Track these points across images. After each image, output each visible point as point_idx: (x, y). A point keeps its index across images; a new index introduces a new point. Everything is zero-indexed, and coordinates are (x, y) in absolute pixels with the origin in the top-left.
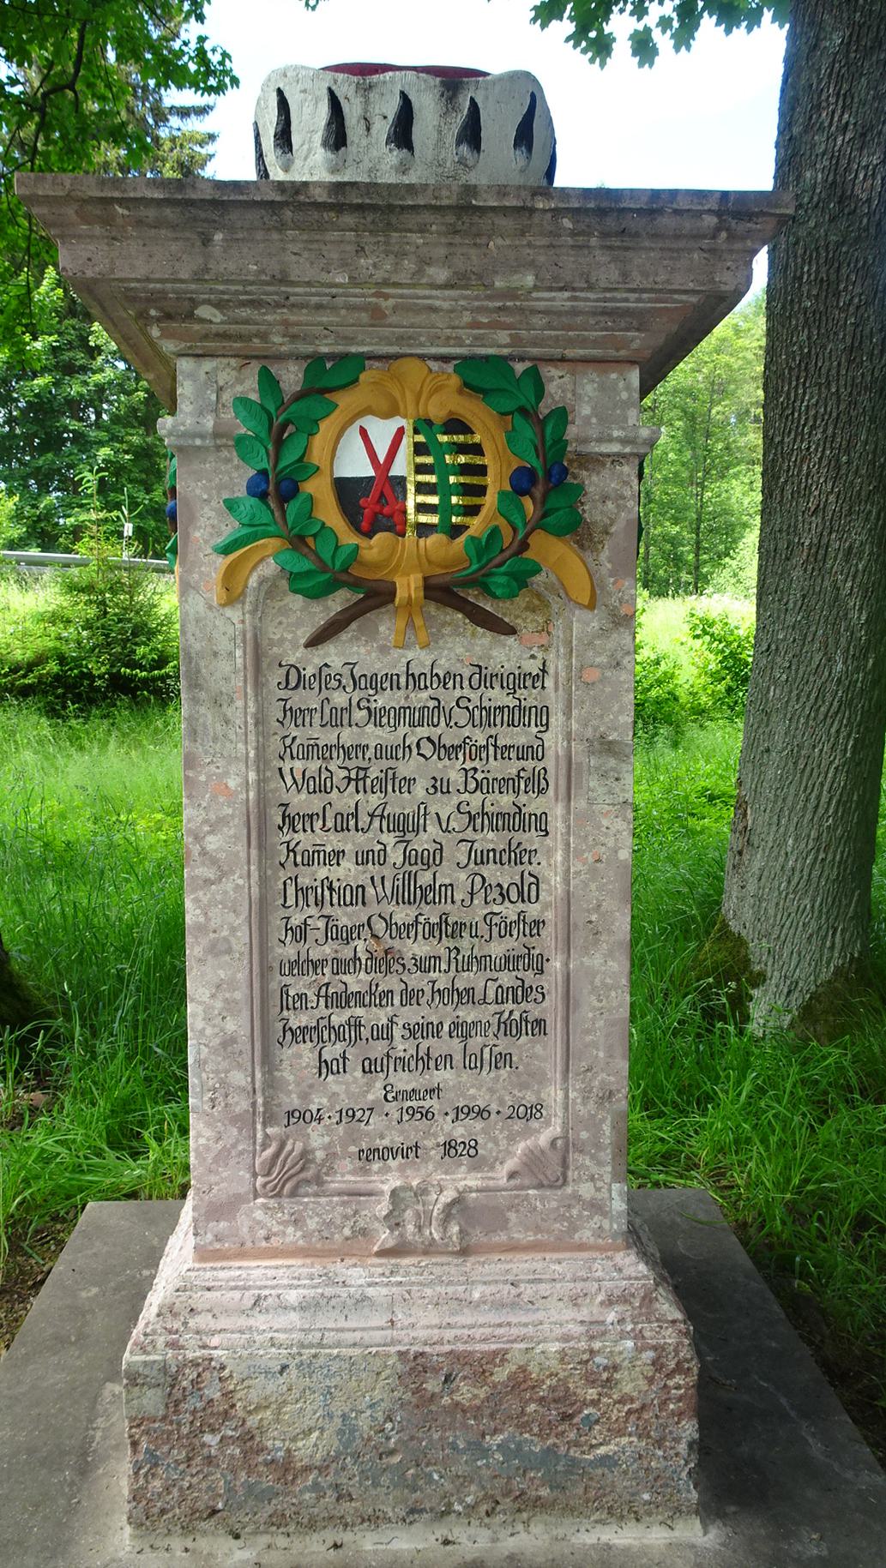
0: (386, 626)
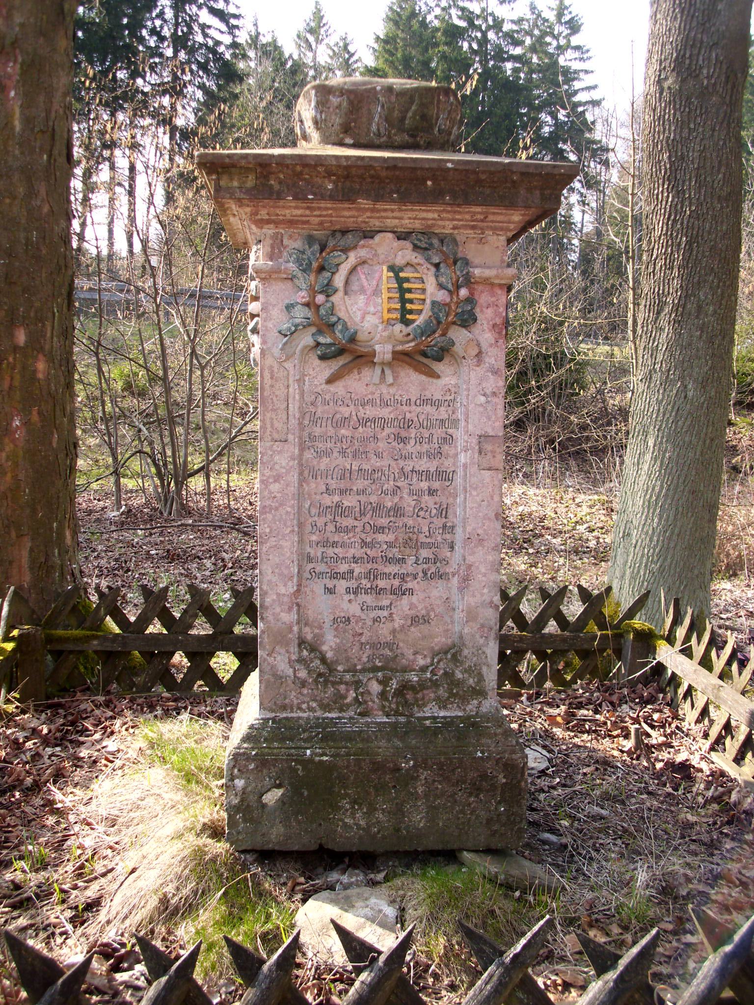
0: (369, 375)
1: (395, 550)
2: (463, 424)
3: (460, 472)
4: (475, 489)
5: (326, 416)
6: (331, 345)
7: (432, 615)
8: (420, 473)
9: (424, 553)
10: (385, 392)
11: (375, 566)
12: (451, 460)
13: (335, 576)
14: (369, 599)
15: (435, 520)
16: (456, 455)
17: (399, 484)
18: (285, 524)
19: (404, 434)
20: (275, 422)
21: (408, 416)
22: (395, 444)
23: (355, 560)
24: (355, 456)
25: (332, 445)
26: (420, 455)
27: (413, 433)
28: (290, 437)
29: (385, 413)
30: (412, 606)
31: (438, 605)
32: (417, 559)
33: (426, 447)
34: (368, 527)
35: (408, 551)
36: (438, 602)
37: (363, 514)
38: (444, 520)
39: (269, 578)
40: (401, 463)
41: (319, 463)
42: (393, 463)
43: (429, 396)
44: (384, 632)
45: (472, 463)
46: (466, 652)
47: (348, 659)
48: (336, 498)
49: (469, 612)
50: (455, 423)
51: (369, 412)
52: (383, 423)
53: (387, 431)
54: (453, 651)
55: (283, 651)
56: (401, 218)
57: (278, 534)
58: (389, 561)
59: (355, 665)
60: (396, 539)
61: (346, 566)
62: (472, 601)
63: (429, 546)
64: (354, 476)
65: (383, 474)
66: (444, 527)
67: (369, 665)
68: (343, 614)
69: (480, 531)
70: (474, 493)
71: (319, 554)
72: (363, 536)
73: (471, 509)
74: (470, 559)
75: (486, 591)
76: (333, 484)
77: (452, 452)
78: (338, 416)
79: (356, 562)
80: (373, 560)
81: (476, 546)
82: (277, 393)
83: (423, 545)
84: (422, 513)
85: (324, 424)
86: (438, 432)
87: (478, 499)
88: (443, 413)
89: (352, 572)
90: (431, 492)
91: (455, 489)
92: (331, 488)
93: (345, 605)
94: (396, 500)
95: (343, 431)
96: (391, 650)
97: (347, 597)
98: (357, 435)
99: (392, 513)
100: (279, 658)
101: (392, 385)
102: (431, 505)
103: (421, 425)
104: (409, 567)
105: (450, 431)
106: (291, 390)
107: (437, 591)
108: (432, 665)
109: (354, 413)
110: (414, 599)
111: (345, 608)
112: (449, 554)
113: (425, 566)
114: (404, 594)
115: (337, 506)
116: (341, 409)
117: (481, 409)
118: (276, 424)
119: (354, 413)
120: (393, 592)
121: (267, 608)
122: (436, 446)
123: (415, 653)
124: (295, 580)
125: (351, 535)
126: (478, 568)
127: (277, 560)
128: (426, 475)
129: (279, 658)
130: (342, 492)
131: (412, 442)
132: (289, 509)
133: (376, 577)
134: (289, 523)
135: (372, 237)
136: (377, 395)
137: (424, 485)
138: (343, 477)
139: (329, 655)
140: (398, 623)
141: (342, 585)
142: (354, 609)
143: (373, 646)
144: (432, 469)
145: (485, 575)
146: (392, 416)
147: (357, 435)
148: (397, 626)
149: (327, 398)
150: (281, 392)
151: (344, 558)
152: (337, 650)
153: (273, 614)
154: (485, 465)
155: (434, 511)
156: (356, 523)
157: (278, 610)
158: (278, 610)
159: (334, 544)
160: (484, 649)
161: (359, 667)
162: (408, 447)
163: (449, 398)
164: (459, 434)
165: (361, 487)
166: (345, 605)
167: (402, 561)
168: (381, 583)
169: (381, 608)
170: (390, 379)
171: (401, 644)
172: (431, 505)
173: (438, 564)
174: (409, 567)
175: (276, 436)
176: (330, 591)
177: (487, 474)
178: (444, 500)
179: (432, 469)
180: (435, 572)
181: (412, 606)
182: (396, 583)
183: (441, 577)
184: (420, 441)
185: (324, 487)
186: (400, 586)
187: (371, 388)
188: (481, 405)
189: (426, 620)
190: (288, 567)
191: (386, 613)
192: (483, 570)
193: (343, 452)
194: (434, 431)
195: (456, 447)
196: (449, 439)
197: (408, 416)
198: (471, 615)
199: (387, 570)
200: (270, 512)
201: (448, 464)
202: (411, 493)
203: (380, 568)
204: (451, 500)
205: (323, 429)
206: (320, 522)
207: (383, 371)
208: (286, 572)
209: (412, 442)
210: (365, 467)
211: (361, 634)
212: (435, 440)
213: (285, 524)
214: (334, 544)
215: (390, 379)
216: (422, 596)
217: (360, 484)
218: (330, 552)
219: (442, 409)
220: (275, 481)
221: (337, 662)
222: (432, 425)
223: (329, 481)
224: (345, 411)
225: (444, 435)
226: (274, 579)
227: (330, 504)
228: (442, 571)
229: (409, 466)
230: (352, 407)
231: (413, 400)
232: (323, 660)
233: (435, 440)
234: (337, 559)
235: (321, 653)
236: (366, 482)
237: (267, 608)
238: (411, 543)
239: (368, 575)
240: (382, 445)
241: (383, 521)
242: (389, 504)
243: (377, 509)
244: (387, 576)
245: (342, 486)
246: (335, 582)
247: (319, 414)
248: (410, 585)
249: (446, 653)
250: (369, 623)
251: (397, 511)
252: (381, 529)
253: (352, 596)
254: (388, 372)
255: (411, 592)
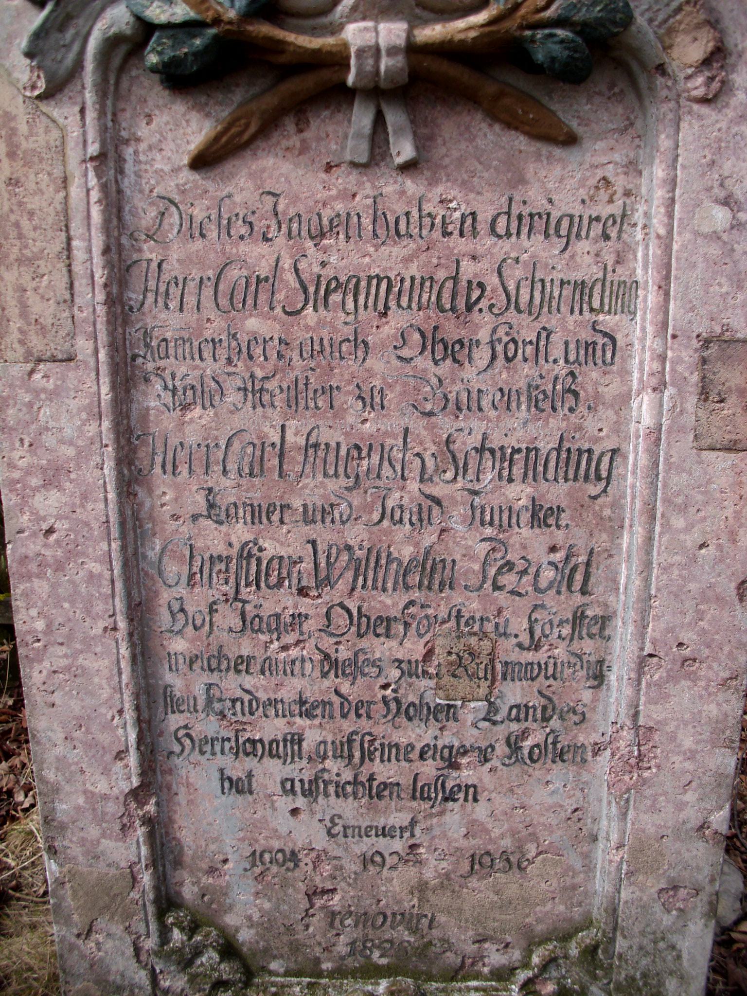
1: (425, 683)
2: (649, 298)
3: (636, 455)
4: (682, 509)
5: (196, 274)
6: (189, 27)
7: (531, 849)
8: (505, 457)
9: (514, 693)
10: (389, 189)
11: (364, 724)
12: (607, 415)
13: (251, 748)
14: (349, 810)
15: (549, 599)
16: (625, 399)
17: (436, 490)
18: (88, 611)
19: (452, 331)
20: (32, 298)
21: (468, 269)
22: (424, 363)
23: (305, 708)
24: (293, 403)
25: (219, 367)
26: (507, 399)
27: (483, 325)
28: (83, 346)
29: (390, 259)
30: (473, 829)
31: (549, 828)
32: (493, 708)
33: (525, 372)
34: (340, 619)
35: (463, 686)
36: (552, 819)
37: (325, 581)
38: (578, 599)
39: (59, 751)
40: (446, 424)
41: (181, 424)
42: (418, 426)
43: (540, 204)
44: (395, 886)
45: (677, 429)
46: (621, 944)
47: (295, 948)
48: (241, 532)
49: (638, 850)
50: (623, 295)
51: (342, 258)
52: (385, 292)
53: (398, 320)
54: (586, 937)
55: (117, 929)
56: (634, 473)
57: (70, 637)
58: (410, 712)
59: (317, 961)
60: (429, 654)
61: (280, 722)
62: (650, 823)
63: (529, 673)
64: (293, 467)
65: (386, 457)
66: (578, 618)
67: (352, 963)
68: (276, 844)
69: (687, 636)
70: (679, 523)
71: (199, 690)
72: (327, 643)
73: (666, 569)
74: (650, 714)
75: (690, 797)
76: (229, 490)
77: (611, 389)
78: (235, 273)
79: (309, 715)
80: (361, 709)
81: (671, 678)
82: (33, 203)
83: (510, 671)
84: (509, 580)
85: (191, 300)
86: (568, 326)
87: (691, 540)
88: (585, 260)
89: (298, 739)
90: (541, 516)
91: (616, 505)
92: (225, 500)
93: (283, 822)
94: (429, 538)
95: (253, 324)
96: (414, 931)
97: (284, 803)
98: (299, 335)
99: (414, 579)
100: (109, 945)
101: (409, 167)
102: (539, 554)
103: (512, 302)
104: (467, 729)
105: (607, 320)
106: (75, 191)
107: (548, 791)
108: (526, 965)
109: (287, 263)
110: (481, 811)
111: (283, 830)
112: (587, 696)
113: (514, 727)
114: (449, 798)
115: (246, 554)
116: (243, 248)
117: (714, 250)
118: (37, 307)
119: (287, 263)
120: (419, 793)
121: (63, 827)
122: (561, 369)
123: (480, 940)
124: (133, 759)
125: (290, 638)
126: (673, 738)
127: (76, 706)
128: (529, 462)
129: (109, 945)
130: (258, 514)
131: (482, 356)
132: (96, 568)
133: (367, 756)
134: (99, 607)
135: (738, 588)
136: (362, 202)
137: (520, 494)
138: (256, 469)
139: (245, 936)
140: (433, 868)
141: (270, 772)
142: (307, 833)
143: (363, 919)
144: (546, 445)
145: (691, 756)
146: (414, 270)
147: (299, 335)
148: (429, 874)
149: (199, 213)
150: (44, 202)
151: (272, 703)
152: (266, 925)
153: (83, 842)
154: (719, 436)
155: (548, 574)
156: (305, 605)
157: (94, 832)
158: (94, 832)
159: (242, 665)
160: (674, 938)
161: (326, 966)
162: (469, 373)
163: (605, 211)
164: (639, 333)
165: (316, 499)
166: (283, 822)
167: (447, 713)
168: (385, 771)
169: (384, 832)
170: (404, 150)
171: (442, 918)
172: (539, 554)
173: (555, 723)
174: (467, 729)
175: (37, 343)
176: (238, 786)
177: (721, 461)
178: (579, 538)
179: (546, 445)
180: (548, 739)
181: (473, 829)
182: (429, 769)
183: (561, 756)
184: (506, 352)
185: (201, 498)
186: (440, 781)
187: (344, 179)
188: (715, 236)
189: (515, 863)
190: (107, 726)
191: (398, 845)
192: (688, 742)
193: (255, 392)
194: (552, 321)
195: (625, 373)
196: (602, 348)
197: (468, 269)
198: (641, 856)
199: (402, 737)
200: (41, 575)
201: (596, 429)
202: (478, 517)
203: (378, 731)
204: (602, 540)
205: (190, 316)
206: (196, 601)
207: (379, 121)
208: (104, 738)
209: (482, 356)
210: (328, 435)
211: (333, 891)
212: (557, 352)
213: (88, 611)
214: (242, 665)
215: (404, 150)
216: (502, 802)
217: (314, 489)
218: (231, 684)
219: (582, 247)
220: (47, 484)
221: (267, 952)
222: (547, 301)
223: (215, 479)
224: (259, 257)
225: (586, 335)
226: (74, 755)
227: (220, 549)
228: (564, 741)
229: (470, 432)
230: (281, 241)
231: (485, 216)
232: (229, 950)
233: (557, 352)
234: (253, 705)
235: (223, 931)
236: (332, 485)
237: (63, 827)
238: (475, 662)
239: (344, 749)
240: (380, 366)
241: (390, 602)
242: (407, 552)
243: (369, 566)
244: (402, 752)
245: (257, 496)
246: (250, 763)
247: (173, 268)
248: (466, 775)
249: (566, 938)
250: (352, 866)
251: (433, 572)
252: (383, 625)
253: (300, 802)
254: (394, 118)
255: (472, 793)
